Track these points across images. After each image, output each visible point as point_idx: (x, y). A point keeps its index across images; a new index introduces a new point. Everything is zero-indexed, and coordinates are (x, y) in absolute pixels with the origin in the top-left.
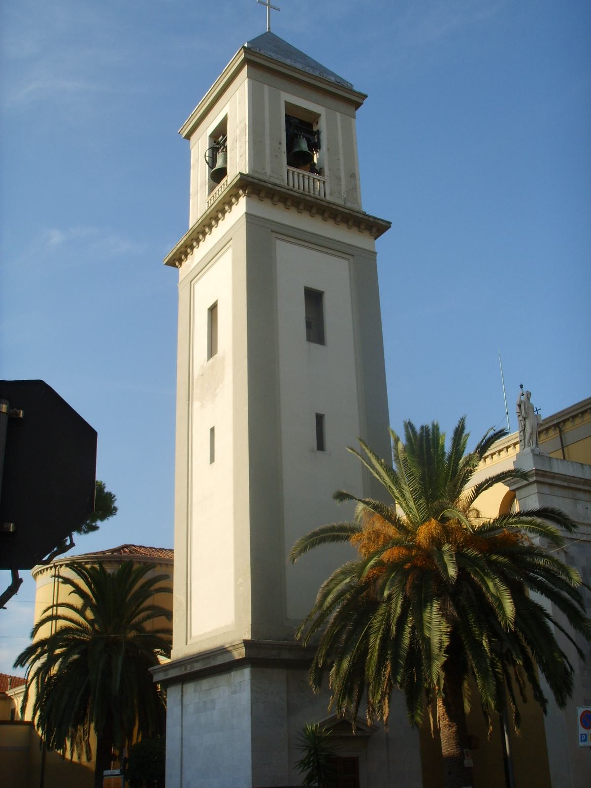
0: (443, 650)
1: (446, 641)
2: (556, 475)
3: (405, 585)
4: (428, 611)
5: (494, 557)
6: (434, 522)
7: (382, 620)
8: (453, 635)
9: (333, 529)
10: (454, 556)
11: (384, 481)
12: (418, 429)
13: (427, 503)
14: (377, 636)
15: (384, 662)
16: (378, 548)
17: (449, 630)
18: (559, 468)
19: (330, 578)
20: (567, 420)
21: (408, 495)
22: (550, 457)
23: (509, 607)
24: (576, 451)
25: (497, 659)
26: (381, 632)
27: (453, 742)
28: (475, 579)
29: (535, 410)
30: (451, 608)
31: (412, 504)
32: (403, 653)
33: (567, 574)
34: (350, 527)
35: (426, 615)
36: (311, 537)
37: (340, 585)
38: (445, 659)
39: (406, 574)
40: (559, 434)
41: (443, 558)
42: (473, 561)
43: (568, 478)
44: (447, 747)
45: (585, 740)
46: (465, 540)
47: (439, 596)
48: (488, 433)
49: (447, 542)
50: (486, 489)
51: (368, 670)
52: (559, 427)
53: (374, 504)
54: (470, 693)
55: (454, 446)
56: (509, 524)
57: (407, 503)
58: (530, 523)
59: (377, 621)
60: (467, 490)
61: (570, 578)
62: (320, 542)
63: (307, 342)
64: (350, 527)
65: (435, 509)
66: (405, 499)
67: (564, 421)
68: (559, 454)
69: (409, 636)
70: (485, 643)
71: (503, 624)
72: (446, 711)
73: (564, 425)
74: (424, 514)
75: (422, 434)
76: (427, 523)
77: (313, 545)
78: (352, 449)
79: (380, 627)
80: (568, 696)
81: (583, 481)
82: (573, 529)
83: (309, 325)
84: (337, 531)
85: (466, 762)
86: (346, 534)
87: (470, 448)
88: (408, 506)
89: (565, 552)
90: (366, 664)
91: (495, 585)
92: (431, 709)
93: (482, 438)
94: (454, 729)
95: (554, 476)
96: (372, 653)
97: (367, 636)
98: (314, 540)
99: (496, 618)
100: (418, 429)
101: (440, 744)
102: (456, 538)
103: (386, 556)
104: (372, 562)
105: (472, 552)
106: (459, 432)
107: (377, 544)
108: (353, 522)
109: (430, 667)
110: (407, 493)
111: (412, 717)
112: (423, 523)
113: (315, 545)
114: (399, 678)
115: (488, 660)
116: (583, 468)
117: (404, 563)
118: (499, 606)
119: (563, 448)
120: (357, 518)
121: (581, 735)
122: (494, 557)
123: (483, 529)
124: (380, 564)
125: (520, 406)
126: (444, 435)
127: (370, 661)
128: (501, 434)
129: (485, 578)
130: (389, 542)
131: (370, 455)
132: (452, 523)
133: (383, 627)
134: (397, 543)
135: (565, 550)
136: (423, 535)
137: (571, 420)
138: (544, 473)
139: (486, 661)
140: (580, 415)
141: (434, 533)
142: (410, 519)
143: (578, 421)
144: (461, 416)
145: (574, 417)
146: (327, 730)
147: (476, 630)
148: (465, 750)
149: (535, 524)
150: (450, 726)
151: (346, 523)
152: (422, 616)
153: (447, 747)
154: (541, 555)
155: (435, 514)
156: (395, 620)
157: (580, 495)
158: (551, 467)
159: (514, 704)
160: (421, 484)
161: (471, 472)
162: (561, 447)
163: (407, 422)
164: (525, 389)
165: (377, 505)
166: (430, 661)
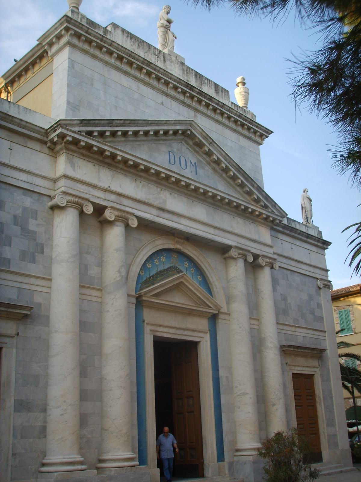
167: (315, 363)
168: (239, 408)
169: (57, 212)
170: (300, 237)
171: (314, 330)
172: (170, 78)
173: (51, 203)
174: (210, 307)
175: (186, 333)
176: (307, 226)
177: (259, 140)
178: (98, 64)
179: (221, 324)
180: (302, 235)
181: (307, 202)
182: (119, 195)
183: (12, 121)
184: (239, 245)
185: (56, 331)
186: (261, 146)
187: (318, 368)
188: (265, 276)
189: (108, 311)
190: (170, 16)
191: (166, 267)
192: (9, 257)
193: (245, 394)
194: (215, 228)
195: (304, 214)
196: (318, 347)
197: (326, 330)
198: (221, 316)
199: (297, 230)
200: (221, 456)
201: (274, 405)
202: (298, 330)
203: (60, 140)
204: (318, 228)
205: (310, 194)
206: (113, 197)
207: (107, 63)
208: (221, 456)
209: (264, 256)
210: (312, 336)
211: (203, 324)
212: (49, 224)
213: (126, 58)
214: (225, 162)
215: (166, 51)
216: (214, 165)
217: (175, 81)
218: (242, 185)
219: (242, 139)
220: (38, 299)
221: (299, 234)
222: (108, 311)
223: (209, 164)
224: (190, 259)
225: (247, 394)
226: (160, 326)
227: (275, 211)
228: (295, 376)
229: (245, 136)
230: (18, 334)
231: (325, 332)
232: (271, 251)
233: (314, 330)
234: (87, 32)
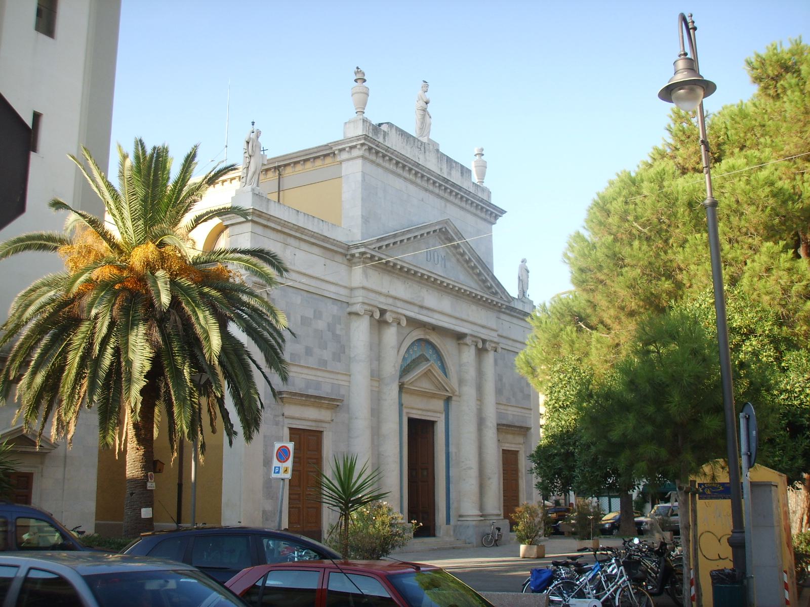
0: (143, 374)
1: (148, 367)
2: (272, 218)
3: (114, 305)
4: (134, 334)
5: (206, 290)
6: (151, 247)
7: (83, 338)
8: (156, 361)
9: (40, 237)
10: (169, 283)
11: (103, 196)
12: (149, 151)
13: (145, 226)
14: (77, 353)
15: (80, 381)
16: (88, 264)
17: (151, 355)
18: (275, 211)
19: (29, 288)
20: (289, 165)
21: (127, 214)
22: (269, 200)
23: (216, 341)
24: (290, 197)
25: (195, 389)
26: (81, 349)
27: (139, 465)
28: (187, 308)
29: (262, 149)
30: (156, 334)
31: (129, 223)
32: (102, 374)
33: (275, 315)
34: (60, 238)
35: (132, 338)
36: (15, 242)
37: (43, 296)
38: (145, 384)
39: (116, 294)
40: (277, 177)
41: (157, 284)
42: (186, 291)
43: (282, 222)
44: (133, 468)
45: (278, 472)
46: (180, 269)
47: (146, 320)
48: (218, 165)
49: (162, 268)
50: (205, 221)
51: (63, 387)
52: (279, 170)
53: (91, 218)
54: (160, 420)
55: (182, 172)
56: (225, 259)
57: (123, 222)
58: (247, 261)
59: (78, 339)
60: (187, 219)
61: (277, 321)
62: (25, 249)
63: (36, 32)
64: (60, 238)
65: (155, 233)
66: (123, 218)
67: (285, 166)
68: (274, 197)
69: (110, 357)
70: (186, 372)
71: (207, 356)
72: (135, 435)
73: (284, 170)
74: (140, 236)
75: (152, 155)
76: (144, 246)
77: (16, 251)
78: (73, 157)
79: (80, 345)
80: (255, 431)
81: (296, 227)
82: (285, 274)
83: (39, 13)
84: (44, 240)
85: (149, 484)
86: (55, 245)
87: (196, 178)
88: (124, 225)
89: (268, 294)
90: (62, 381)
91: (205, 317)
92: (118, 431)
93: (211, 170)
94: (141, 452)
95: (270, 218)
96: (69, 370)
97: (64, 353)
98: (18, 246)
99: (201, 349)
100: (149, 151)
101: (125, 465)
102: (171, 265)
103: (96, 274)
104: (82, 278)
105: (185, 282)
106: (190, 161)
107: (88, 260)
108: (63, 232)
109: (129, 389)
110: (126, 213)
111: (104, 437)
112: (139, 244)
113: (20, 250)
114: (95, 398)
115: (187, 389)
116: (298, 215)
117: (115, 283)
118: (206, 338)
119: (279, 191)
120: (67, 229)
121: (275, 467)
122: (206, 290)
123: (198, 261)
124: (89, 281)
125: (248, 143)
126: (172, 159)
127: (66, 379)
128: (231, 168)
129: (196, 309)
130: (99, 260)
131: (92, 166)
132: (168, 250)
133: (83, 345)
134: (110, 263)
135: (269, 292)
136: (138, 257)
137: (292, 165)
138: (260, 213)
139: (186, 390)
140: (302, 163)
141: (150, 257)
142: (124, 239)
143: (299, 167)
144: (195, 143)
145: (296, 163)
146: (8, 443)
147: (179, 359)
148: (149, 473)
149: (250, 263)
150: (138, 449)
151: (56, 233)
152: (128, 339)
153: (133, 468)
154: (251, 294)
155: (154, 238)
156: (100, 340)
157: (291, 241)
158: (268, 210)
159: (202, 433)
160: (142, 205)
161: (195, 201)
162: (277, 190)
163: (138, 139)
164: (256, 127)
165: (94, 220)
166: (130, 384)
167: (520, 439)
168: (464, 480)
169: (353, 317)
170: (518, 315)
171: (522, 408)
172: (432, 176)
173: (349, 310)
174: (447, 391)
175: (430, 414)
176: (522, 301)
177: (492, 220)
178: (380, 170)
179: (453, 405)
180: (520, 314)
181: (524, 273)
182: (395, 298)
183: (328, 241)
184: (476, 334)
185: (356, 418)
186: (493, 226)
187: (522, 444)
188: (490, 358)
189: (386, 400)
190: (428, 96)
191: (417, 355)
192: (326, 359)
193: (470, 468)
194: (457, 318)
195: (521, 286)
196: (524, 425)
197: (532, 408)
198: (454, 398)
199: (517, 309)
200: (448, 521)
201: (489, 479)
202: (510, 408)
203: (361, 256)
204: (532, 302)
205: (529, 265)
206: (390, 301)
207: (386, 169)
208: (448, 521)
209: (491, 341)
210: (520, 414)
211: (439, 405)
212: (348, 328)
213: (402, 163)
214: (469, 255)
215: (425, 140)
216: (458, 256)
217: (435, 177)
218: (479, 274)
219: (479, 221)
220: (343, 392)
221: (518, 313)
222: (386, 400)
223: (455, 255)
224: (433, 347)
225: (472, 468)
226: (413, 408)
227: (503, 297)
228: (505, 452)
229: (482, 218)
230: (332, 420)
231: (531, 409)
232: (494, 334)
233: (522, 408)
234: (377, 146)
